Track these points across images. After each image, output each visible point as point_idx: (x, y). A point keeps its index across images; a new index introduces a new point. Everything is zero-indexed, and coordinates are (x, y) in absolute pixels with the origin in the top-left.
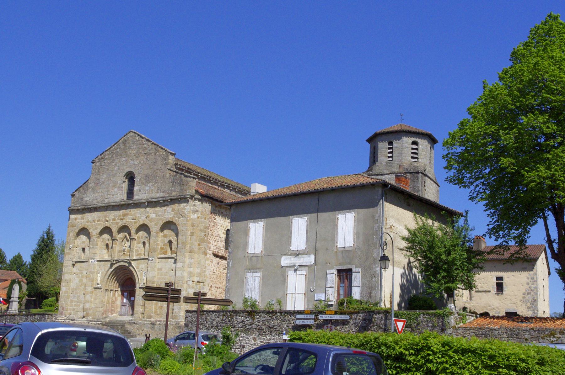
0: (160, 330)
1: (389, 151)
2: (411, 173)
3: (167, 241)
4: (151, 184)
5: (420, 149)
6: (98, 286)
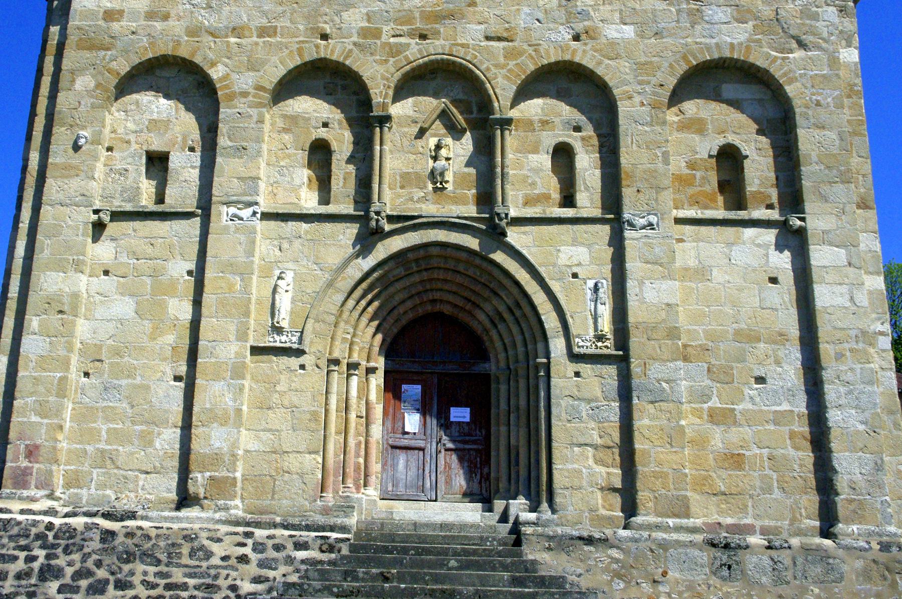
0: (779, 580)
6: (279, 341)
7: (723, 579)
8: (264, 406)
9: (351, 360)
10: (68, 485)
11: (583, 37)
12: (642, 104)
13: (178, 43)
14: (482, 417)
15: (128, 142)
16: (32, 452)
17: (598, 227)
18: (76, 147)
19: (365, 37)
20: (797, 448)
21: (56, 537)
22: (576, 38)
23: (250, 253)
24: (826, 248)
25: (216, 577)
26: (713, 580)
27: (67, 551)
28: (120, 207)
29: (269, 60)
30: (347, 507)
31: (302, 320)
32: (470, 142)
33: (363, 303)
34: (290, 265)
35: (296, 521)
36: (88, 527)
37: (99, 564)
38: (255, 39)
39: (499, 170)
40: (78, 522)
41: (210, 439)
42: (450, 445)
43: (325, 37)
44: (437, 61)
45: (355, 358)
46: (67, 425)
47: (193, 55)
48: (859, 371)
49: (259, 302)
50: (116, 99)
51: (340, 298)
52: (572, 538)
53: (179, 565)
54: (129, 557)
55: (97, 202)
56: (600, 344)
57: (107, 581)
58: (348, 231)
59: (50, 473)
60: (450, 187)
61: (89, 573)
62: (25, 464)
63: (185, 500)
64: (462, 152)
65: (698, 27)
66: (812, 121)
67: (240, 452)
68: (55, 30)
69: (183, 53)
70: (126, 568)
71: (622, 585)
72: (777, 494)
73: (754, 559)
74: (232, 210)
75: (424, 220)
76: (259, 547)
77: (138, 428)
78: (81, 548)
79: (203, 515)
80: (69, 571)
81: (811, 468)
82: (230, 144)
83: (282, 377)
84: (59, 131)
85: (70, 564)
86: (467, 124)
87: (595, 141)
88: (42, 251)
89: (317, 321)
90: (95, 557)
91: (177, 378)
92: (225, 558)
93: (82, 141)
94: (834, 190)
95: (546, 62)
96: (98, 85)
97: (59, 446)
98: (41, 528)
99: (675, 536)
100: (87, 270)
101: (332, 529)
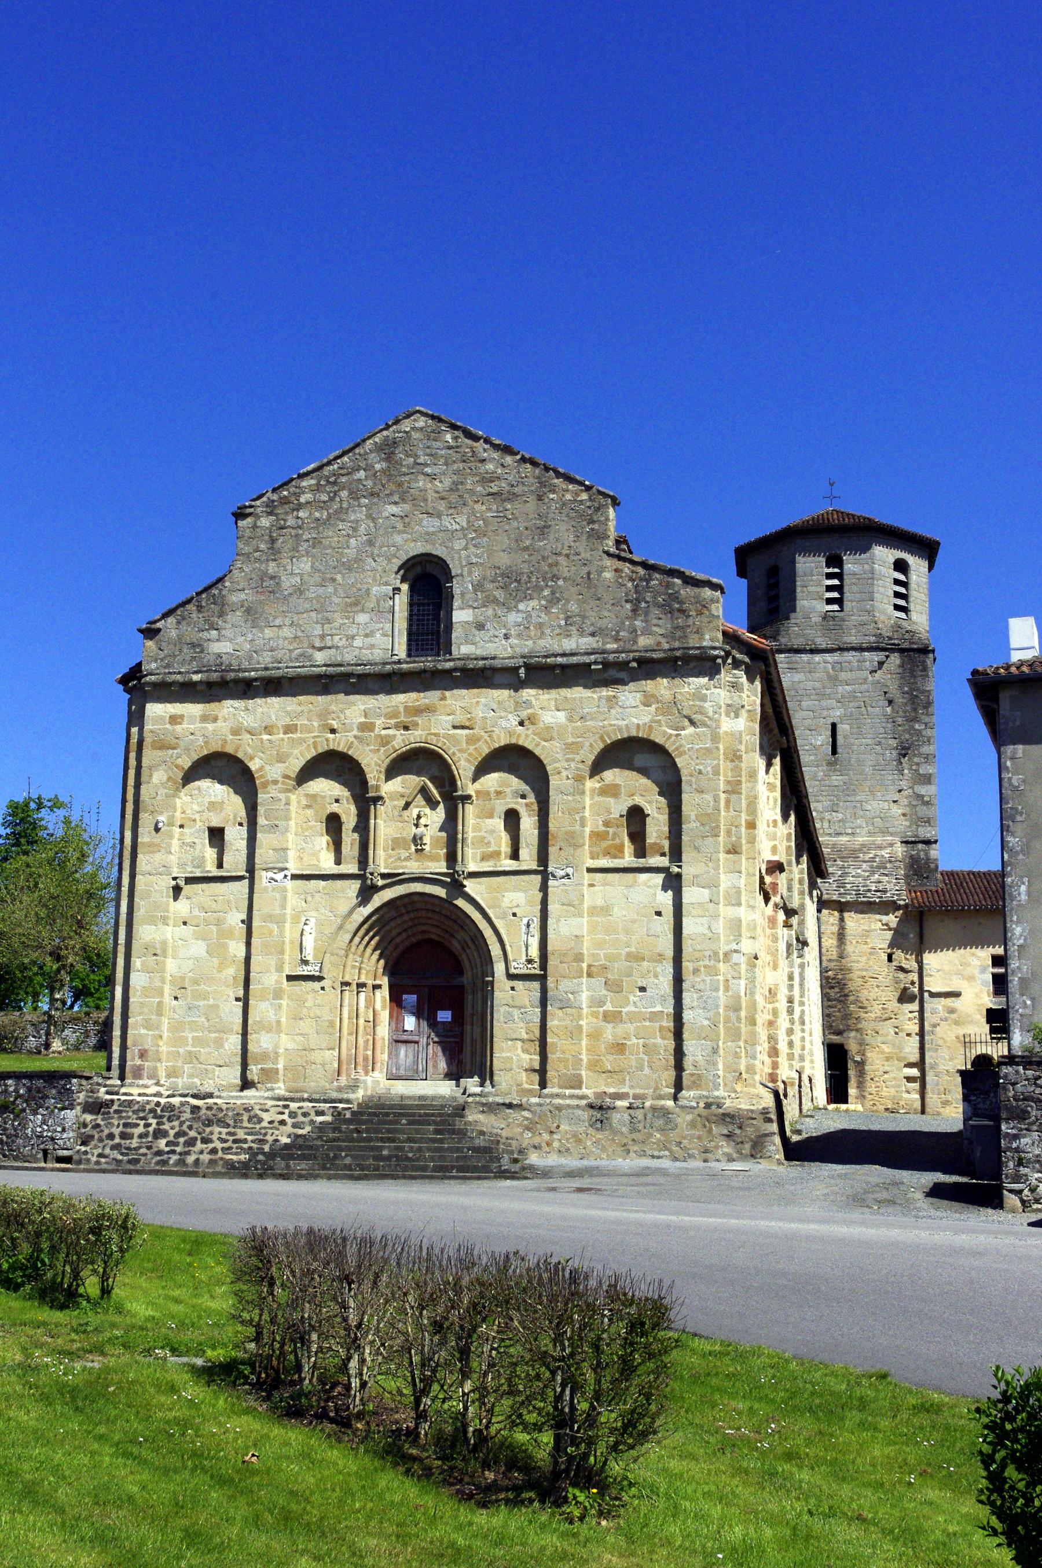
0: (634, 1130)
1: (830, 582)
2: (902, 651)
3: (619, 807)
4: (534, 603)
5: (913, 585)
6: (306, 970)
7: (597, 1129)
8: (297, 1018)
9: (360, 981)
10: (168, 1076)
11: (526, 723)
12: (568, 778)
13: (225, 741)
14: (459, 1018)
15: (194, 820)
16: (143, 1054)
17: (533, 876)
18: (157, 830)
19: (363, 731)
20: (663, 1038)
21: (162, 1111)
22: (521, 724)
23: (283, 907)
24: (694, 889)
25: (265, 1134)
26: (591, 1131)
27: (170, 1120)
28: (191, 872)
29: (292, 753)
30: (354, 1087)
31: (321, 953)
32: (443, 811)
33: (367, 938)
34: (313, 914)
35: (317, 1096)
36: (182, 1104)
37: (190, 1128)
38: (281, 735)
39: (460, 836)
40: (176, 1101)
41: (260, 1042)
42: (436, 1039)
43: (333, 731)
44: (416, 748)
45: (363, 980)
46: (165, 1035)
47: (237, 751)
48: (708, 982)
49: (292, 942)
50: (184, 786)
51: (348, 937)
52: (498, 1104)
53: (242, 1128)
54: (209, 1123)
55: (175, 869)
56: (530, 966)
57: (196, 1139)
58: (353, 886)
59: (156, 1068)
60: (427, 848)
61: (185, 1134)
62: (138, 1062)
63: (246, 1084)
64: (437, 819)
65: (613, 711)
66: (694, 786)
67: (281, 1051)
68: (135, 730)
69: (229, 749)
70: (208, 1130)
71: (530, 1135)
72: (647, 1071)
73: (618, 1116)
74: (270, 874)
75: (407, 876)
76: (293, 1115)
77: (213, 1035)
78: (179, 1118)
79: (257, 1094)
80: (172, 1133)
81: (672, 1052)
82: (267, 823)
83: (309, 996)
84: (143, 816)
85: (172, 1128)
86: (441, 796)
87: (535, 807)
88: (139, 909)
89: (332, 955)
90: (188, 1123)
91: (237, 999)
92: (270, 1123)
93: (160, 825)
94: (705, 842)
95: (497, 746)
96: (169, 779)
97: (161, 1049)
98: (152, 1105)
99: (568, 1102)
100: (171, 922)
101: (340, 1101)
